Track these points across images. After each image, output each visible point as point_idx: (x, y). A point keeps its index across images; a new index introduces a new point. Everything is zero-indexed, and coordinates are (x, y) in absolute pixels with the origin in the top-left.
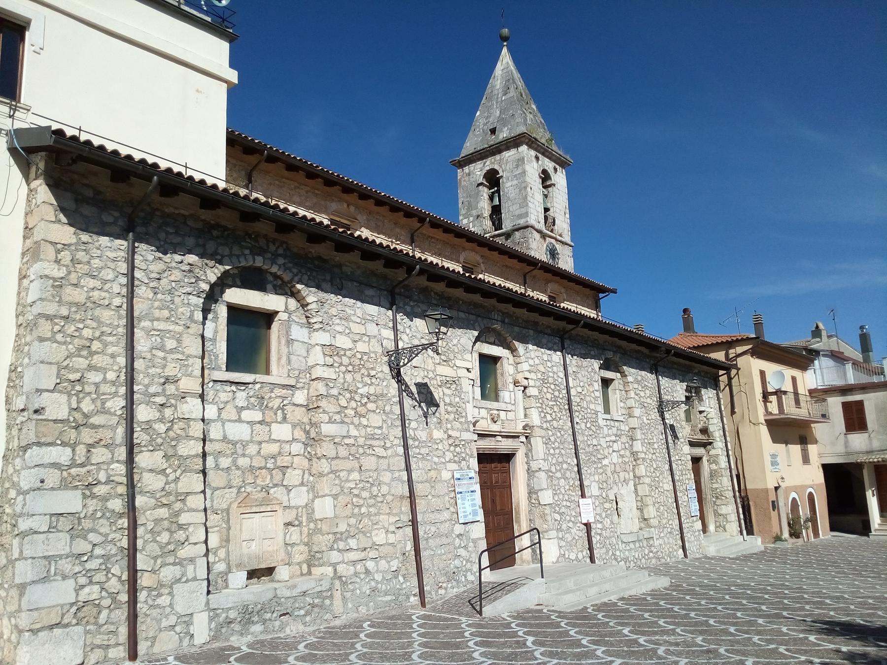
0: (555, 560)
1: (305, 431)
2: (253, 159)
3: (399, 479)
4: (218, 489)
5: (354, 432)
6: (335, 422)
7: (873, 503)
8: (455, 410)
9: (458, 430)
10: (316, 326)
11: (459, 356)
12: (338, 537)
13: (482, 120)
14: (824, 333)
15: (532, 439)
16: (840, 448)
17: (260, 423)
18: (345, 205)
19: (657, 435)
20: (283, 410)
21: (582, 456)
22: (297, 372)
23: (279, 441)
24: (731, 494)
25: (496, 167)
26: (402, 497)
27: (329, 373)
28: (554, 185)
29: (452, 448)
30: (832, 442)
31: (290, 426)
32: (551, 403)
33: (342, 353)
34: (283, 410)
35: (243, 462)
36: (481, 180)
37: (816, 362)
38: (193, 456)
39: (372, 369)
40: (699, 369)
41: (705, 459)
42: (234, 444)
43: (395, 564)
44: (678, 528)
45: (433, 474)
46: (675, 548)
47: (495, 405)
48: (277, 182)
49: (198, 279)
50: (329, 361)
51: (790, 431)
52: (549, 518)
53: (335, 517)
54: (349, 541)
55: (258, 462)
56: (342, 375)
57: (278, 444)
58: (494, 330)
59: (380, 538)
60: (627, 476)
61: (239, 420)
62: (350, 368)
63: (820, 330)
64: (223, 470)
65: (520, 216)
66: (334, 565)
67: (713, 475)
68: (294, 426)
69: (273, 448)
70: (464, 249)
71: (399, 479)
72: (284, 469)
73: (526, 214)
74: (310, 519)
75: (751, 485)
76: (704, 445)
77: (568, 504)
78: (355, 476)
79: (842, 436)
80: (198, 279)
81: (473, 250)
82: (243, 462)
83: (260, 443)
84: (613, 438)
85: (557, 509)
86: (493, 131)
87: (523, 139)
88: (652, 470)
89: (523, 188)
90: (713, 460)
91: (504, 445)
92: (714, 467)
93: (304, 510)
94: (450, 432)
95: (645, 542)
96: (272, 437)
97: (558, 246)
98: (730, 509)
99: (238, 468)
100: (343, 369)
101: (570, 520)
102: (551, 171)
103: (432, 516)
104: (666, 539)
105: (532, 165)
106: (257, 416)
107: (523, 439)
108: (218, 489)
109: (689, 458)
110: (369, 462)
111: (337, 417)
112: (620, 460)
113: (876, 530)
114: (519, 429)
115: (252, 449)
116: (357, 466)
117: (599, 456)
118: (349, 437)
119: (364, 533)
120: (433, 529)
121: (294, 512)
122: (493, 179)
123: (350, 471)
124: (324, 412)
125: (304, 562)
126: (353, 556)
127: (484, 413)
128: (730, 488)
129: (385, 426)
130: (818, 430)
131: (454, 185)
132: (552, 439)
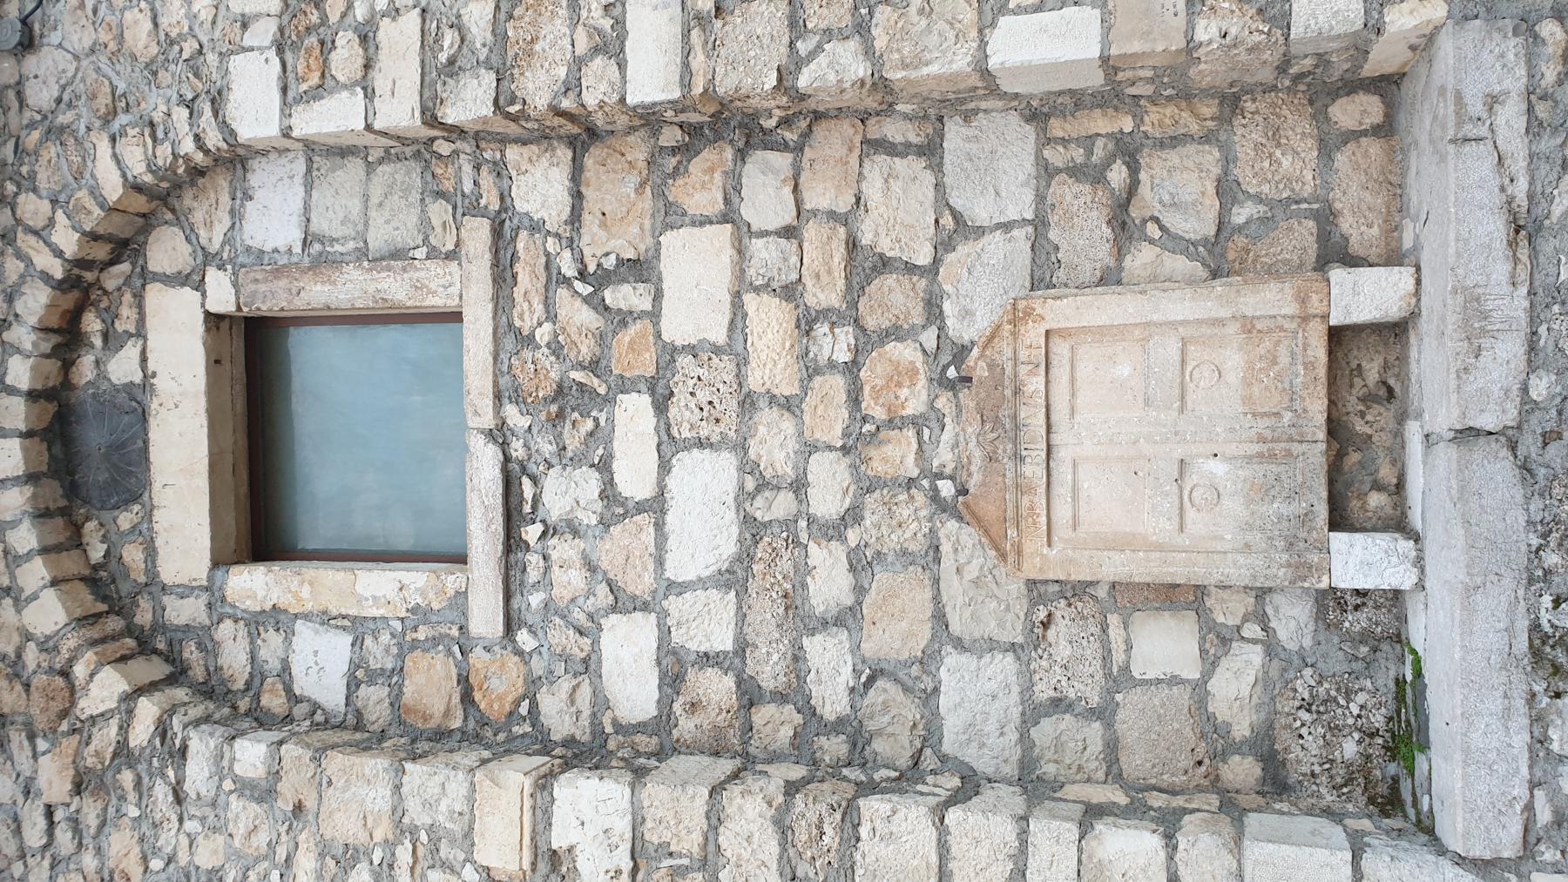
1: (686, 151)
4: (940, 618)
17: (661, 406)
20: (602, 279)
23: (737, 295)
31: (667, 239)
34: (602, 279)
35: (829, 490)
38: (783, 845)
42: (752, 529)
49: (123, 752)
55: (828, 416)
57: (750, 300)
61: (657, 506)
64: (860, 590)
68: (671, 216)
69: (769, 322)
72: (865, 266)
80: (123, 752)
82: (829, 490)
83: (748, 403)
93: (1057, 128)
96: (719, 336)
99: (853, 515)
106: (633, 416)
108: (940, 618)
115: (774, 442)
121: (1068, 192)
125: (1321, 117)
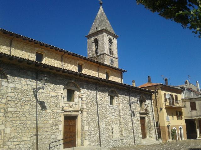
0: (87, 145)
2: (12, 37)
3: (33, 123)
5: (19, 110)
6: (13, 107)
7: (198, 131)
8: (55, 104)
9: (56, 109)
10: (9, 82)
11: (59, 90)
12: (10, 138)
13: (95, 25)
14: (188, 83)
15: (83, 112)
16: (189, 115)
18: (41, 49)
19: (128, 112)
21: (100, 117)
22: (3, 94)
24: (154, 127)
25: (97, 38)
26: (34, 128)
27: (13, 95)
28: (113, 43)
29: (53, 115)
30: (187, 113)
32: (90, 102)
33: (18, 89)
36: (93, 41)
37: (184, 91)
39: (28, 93)
40: (144, 94)
41: (146, 118)
43: (29, 146)
44: (133, 137)
45: (46, 122)
46: (132, 142)
47: (72, 103)
48: (20, 43)
50: (13, 91)
51: (175, 111)
52: (86, 134)
53: (10, 133)
54: (14, 139)
56: (17, 95)
58: (73, 83)
59: (25, 138)
60: (117, 122)
62: (20, 93)
63: (187, 82)
65: (103, 51)
66: (9, 146)
67: (149, 122)
70: (79, 60)
71: (33, 123)
73: (104, 50)
74: (4, 133)
75: (161, 125)
76: (146, 114)
77: (94, 130)
78: (18, 122)
79: (190, 112)
81: (82, 60)
84: (113, 112)
85: (89, 131)
86: (97, 28)
87: (104, 31)
88: (125, 121)
89: (103, 43)
90: (149, 118)
91: (74, 114)
92: (149, 120)
94: (53, 110)
95: (120, 141)
97: (113, 59)
98: (154, 132)
100: (17, 93)
101: (94, 134)
102: (112, 39)
103: (44, 133)
104: (128, 140)
105: (106, 38)
107: (80, 112)
109: (139, 117)
110: (23, 118)
111: (14, 106)
112: (115, 118)
113: (198, 138)
114: (79, 109)
116: (19, 119)
117: (106, 117)
118: (17, 112)
119: (20, 137)
120: (44, 136)
122: (96, 41)
123: (16, 121)
124: (9, 105)
126: (15, 143)
127: (67, 105)
128: (154, 126)
129: (30, 109)
130: (184, 110)
131: (87, 42)
132: (90, 112)
